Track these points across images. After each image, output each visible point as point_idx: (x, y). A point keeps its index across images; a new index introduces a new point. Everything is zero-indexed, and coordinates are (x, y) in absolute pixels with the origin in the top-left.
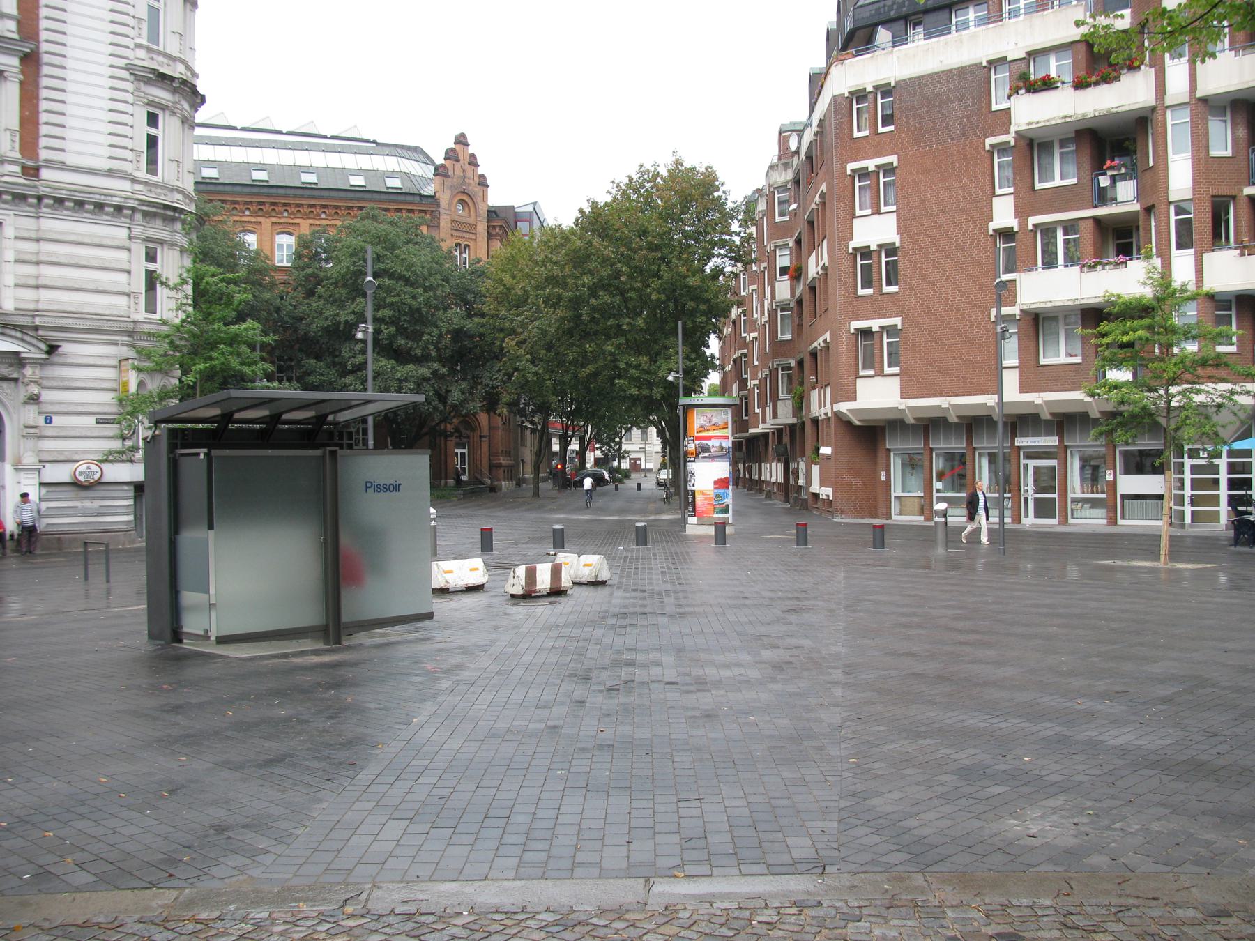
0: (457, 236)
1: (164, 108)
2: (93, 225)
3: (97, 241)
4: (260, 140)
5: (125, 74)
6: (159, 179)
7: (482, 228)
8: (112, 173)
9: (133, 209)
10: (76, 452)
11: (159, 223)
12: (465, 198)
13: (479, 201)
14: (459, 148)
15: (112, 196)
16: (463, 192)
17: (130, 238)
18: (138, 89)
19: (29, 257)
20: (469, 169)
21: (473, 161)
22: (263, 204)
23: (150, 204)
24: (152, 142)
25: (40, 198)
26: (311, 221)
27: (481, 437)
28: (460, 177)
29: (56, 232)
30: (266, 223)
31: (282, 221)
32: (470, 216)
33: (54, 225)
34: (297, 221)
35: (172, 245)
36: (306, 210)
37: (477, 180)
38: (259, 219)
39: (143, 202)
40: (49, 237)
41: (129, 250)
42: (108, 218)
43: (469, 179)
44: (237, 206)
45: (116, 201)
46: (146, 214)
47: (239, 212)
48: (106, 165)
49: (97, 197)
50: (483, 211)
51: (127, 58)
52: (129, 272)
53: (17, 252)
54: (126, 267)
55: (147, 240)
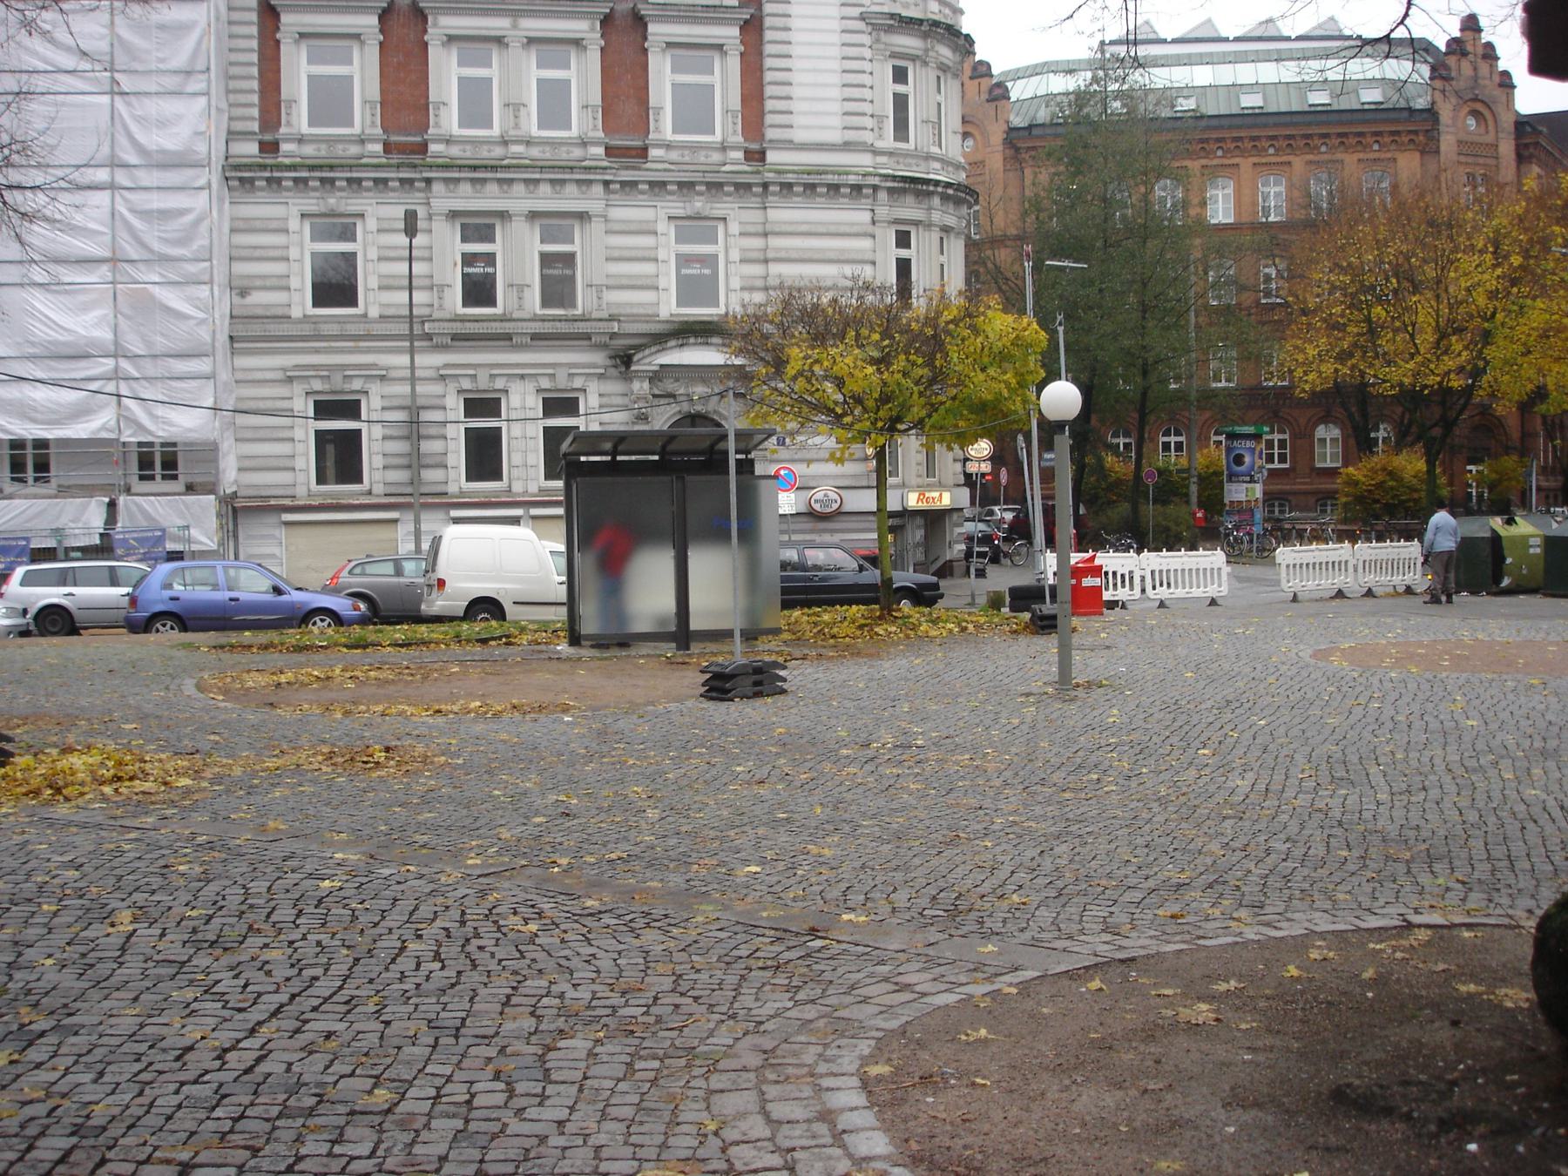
0: (1467, 163)
1: (913, 58)
2: (852, 212)
3: (833, 229)
4: (1189, 55)
5: (861, 25)
6: (911, 145)
7: (1507, 148)
8: (847, 146)
9: (875, 188)
10: (814, 477)
11: (910, 199)
12: (1479, 107)
13: (1500, 109)
14: (1469, 35)
15: (847, 174)
16: (1476, 100)
17: (874, 223)
18: (878, 41)
19: (755, 255)
20: (1484, 68)
22: (1240, 139)
23: (894, 178)
24: (901, 102)
25: (765, 186)
29: (785, 223)
30: (1246, 164)
31: (1215, 162)
33: (784, 214)
34: (1339, 156)
35: (929, 226)
36: (1249, 145)
37: (1497, 79)
39: (886, 177)
40: (777, 230)
41: (874, 237)
42: (846, 200)
43: (1484, 78)
45: (852, 179)
46: (891, 191)
48: (836, 137)
49: (830, 177)
50: (1507, 122)
51: (863, 6)
52: (874, 263)
53: (743, 250)
54: (869, 256)
55: (897, 221)
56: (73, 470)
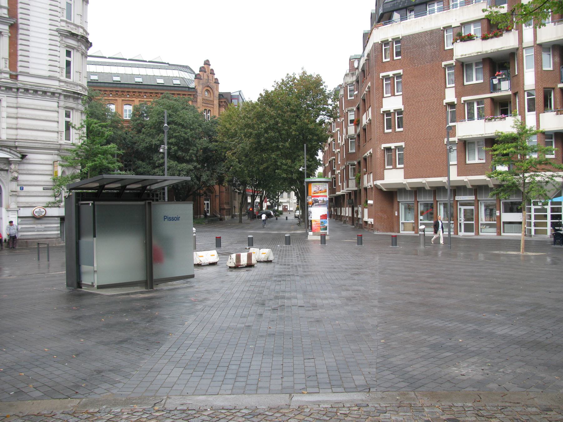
0: (205, 106)
1: (73, 48)
2: (42, 101)
3: (43, 108)
4: (117, 63)
5: (56, 33)
6: (71, 80)
7: (216, 102)
8: (50, 78)
9: (60, 94)
11: (71, 100)
12: (209, 89)
13: (215, 90)
14: (206, 66)
15: (50, 88)
16: (208, 86)
17: (58, 107)
18: (62, 40)
19: (13, 115)
20: (210, 76)
21: (212, 72)
22: (118, 91)
23: (67, 91)
24: (68, 64)
25: (18, 89)
26: (140, 99)
27: (216, 196)
28: (206, 80)
29: (25, 104)
30: (120, 100)
31: (127, 99)
32: (211, 97)
33: (24, 101)
34: (133, 99)
36: (137, 94)
37: (214, 81)
38: (116, 98)
39: (64, 91)
40: (22, 106)
41: (58, 112)
42: (49, 98)
43: (210, 80)
44: (106, 92)
45: (52, 90)
47: (107, 95)
48: (47, 74)
49: (44, 88)
50: (217, 95)
51: (57, 26)
52: (58, 122)
53: (8, 113)
54: (56, 120)
55: (66, 107)
56: (114, 407)
